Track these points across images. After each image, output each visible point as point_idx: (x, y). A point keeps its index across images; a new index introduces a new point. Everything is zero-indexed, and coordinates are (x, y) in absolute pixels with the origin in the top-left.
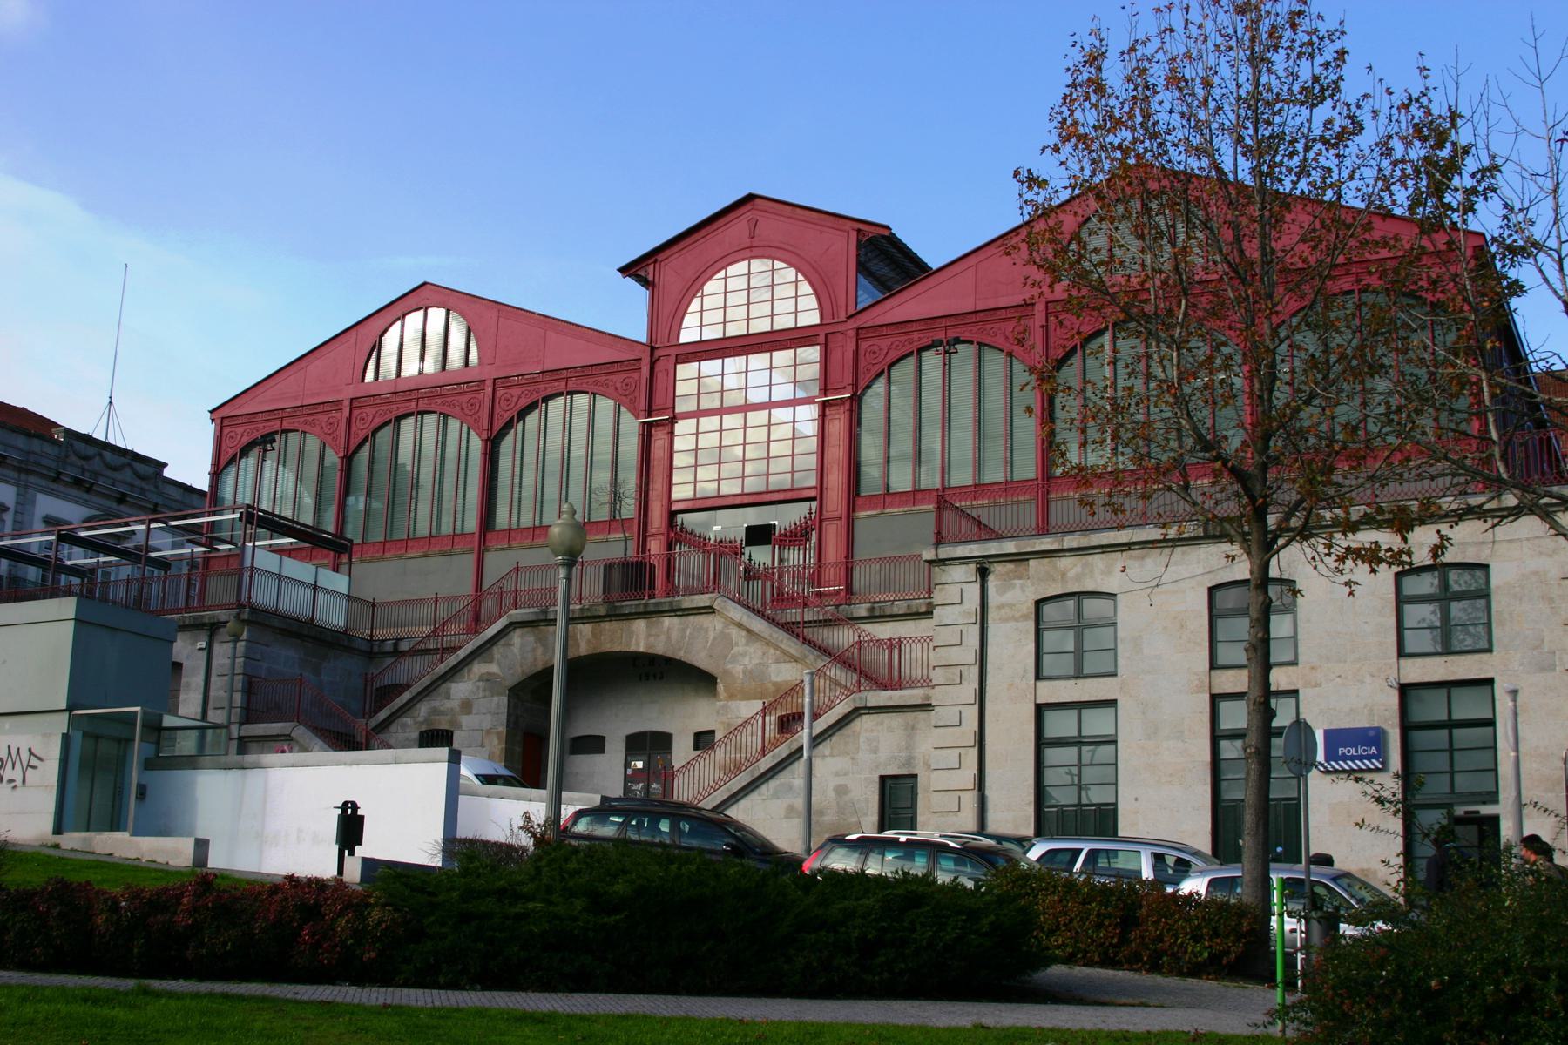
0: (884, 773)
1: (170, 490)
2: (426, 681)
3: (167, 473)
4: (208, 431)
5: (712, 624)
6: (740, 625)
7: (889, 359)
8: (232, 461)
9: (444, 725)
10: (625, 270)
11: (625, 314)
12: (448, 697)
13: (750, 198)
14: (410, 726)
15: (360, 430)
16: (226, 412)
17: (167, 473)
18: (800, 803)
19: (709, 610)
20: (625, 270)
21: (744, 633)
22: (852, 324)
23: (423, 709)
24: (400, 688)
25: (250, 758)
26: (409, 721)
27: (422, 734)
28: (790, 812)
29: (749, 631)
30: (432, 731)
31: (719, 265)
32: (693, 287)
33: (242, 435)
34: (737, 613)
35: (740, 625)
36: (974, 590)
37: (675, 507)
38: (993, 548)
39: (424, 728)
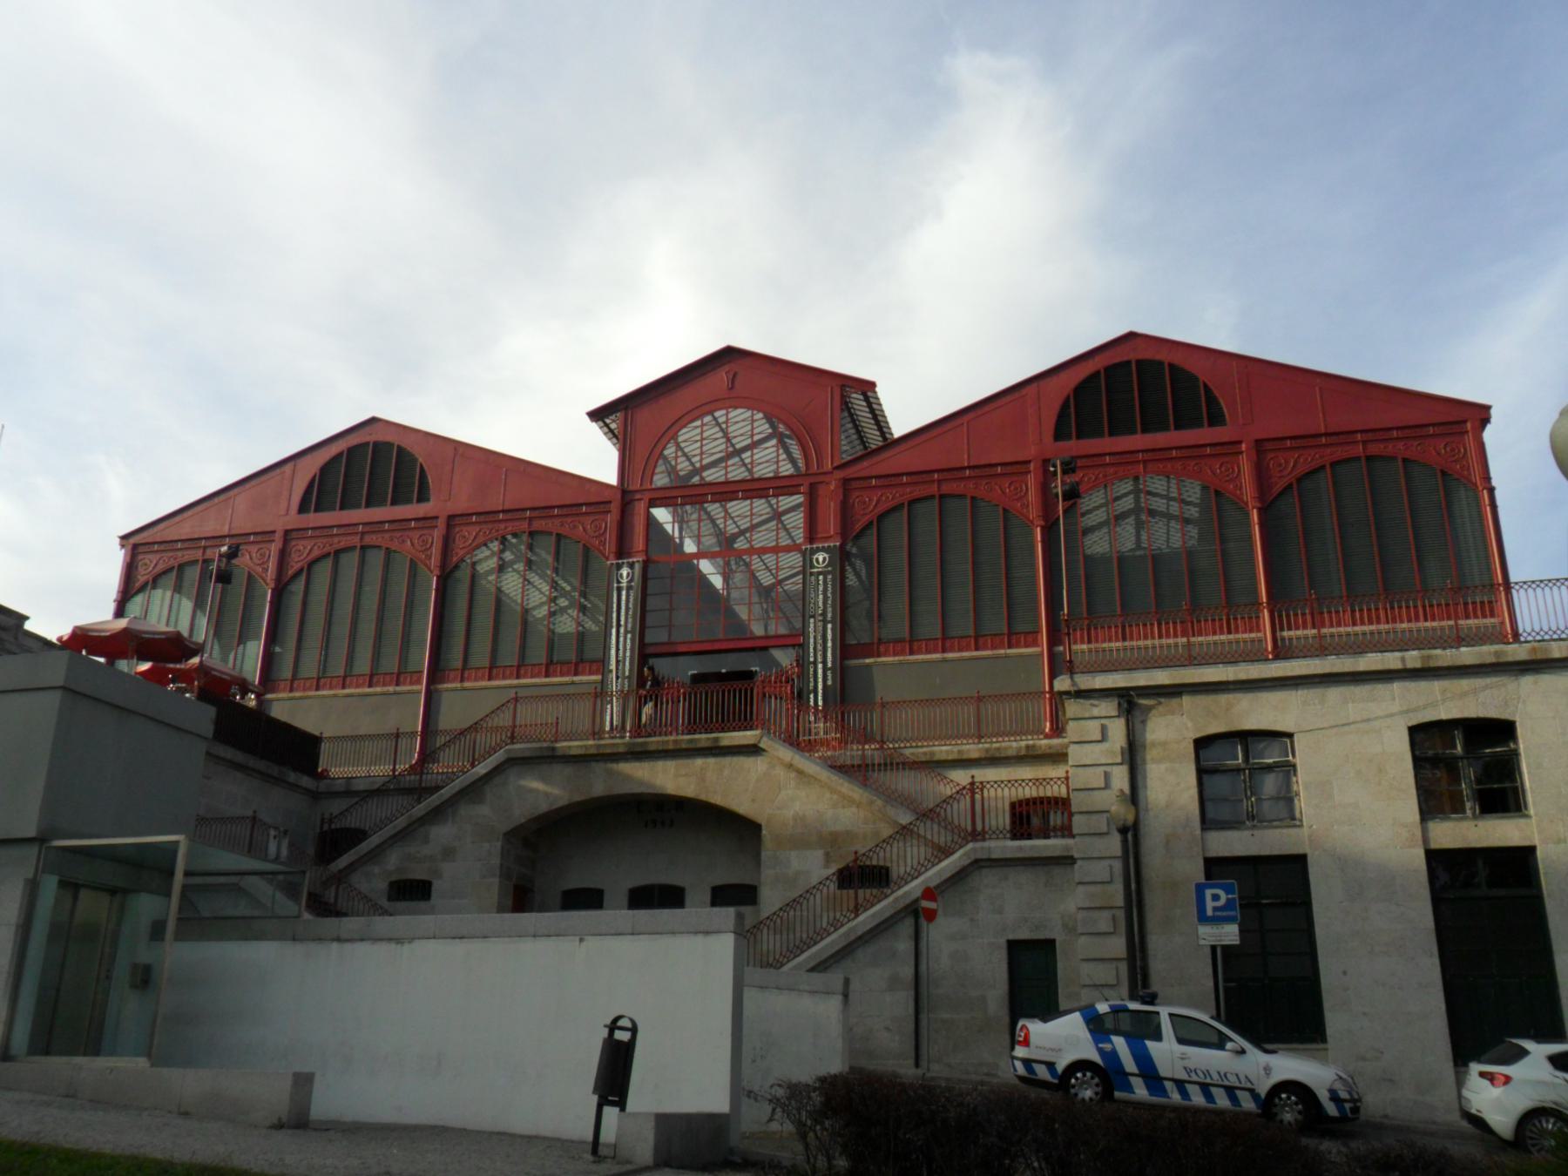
0: (1011, 937)
1: (31, 643)
2: (401, 822)
3: (28, 626)
4: (116, 560)
5: (754, 767)
6: (790, 766)
7: (880, 510)
8: (142, 589)
9: (418, 873)
10: (597, 415)
11: (597, 460)
12: (426, 841)
13: (728, 355)
14: (373, 882)
15: (296, 562)
16: (133, 540)
17: (28, 626)
18: (908, 972)
19: (753, 750)
20: (597, 415)
21: (793, 775)
22: (840, 474)
23: (393, 860)
24: (358, 835)
25: (1298, 815)
26: (376, 870)
27: (392, 884)
28: (894, 983)
29: (800, 772)
30: (405, 881)
31: (696, 413)
32: (670, 432)
33: (150, 564)
34: (786, 753)
35: (790, 766)
36: (1118, 729)
37: (650, 650)
38: (1141, 679)
39: (394, 878)
